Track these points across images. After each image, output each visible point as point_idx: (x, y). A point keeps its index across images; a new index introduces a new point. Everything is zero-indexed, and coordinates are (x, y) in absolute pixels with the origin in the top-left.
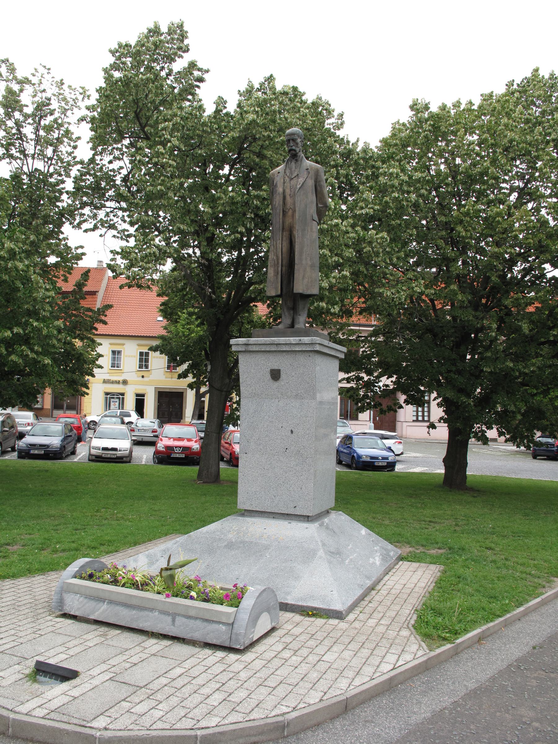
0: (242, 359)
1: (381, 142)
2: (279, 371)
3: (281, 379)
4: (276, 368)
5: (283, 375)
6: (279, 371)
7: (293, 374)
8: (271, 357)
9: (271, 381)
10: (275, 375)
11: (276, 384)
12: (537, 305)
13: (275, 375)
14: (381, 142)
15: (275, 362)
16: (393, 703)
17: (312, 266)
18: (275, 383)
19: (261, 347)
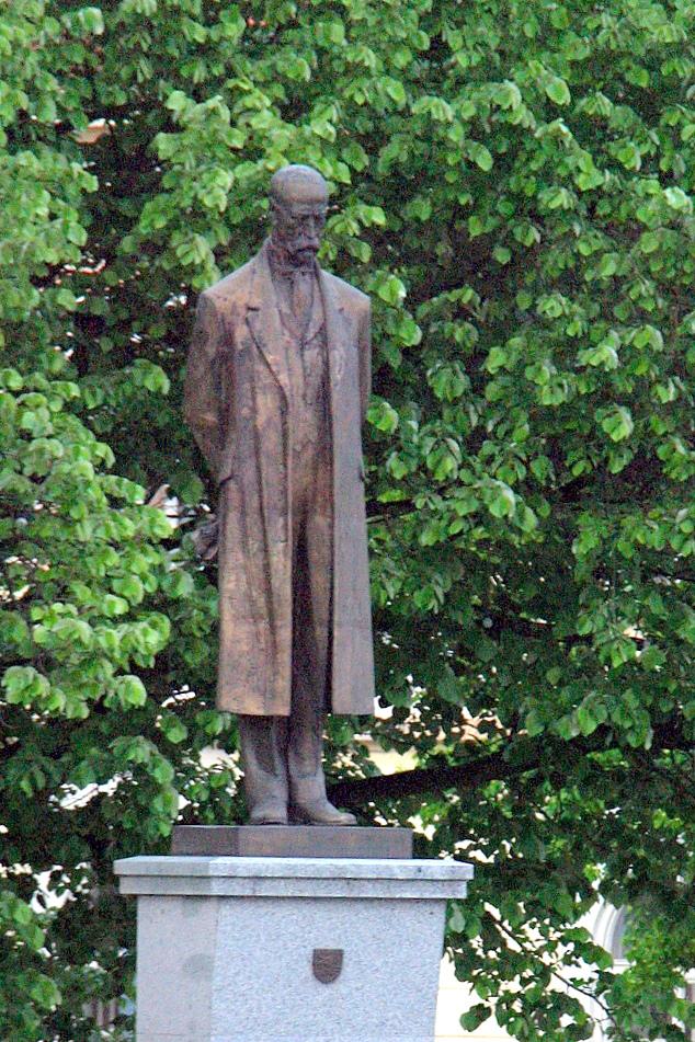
0: (144, 910)
1: (501, 1026)
2: (338, 955)
3: (341, 977)
4: (332, 946)
5: (348, 969)
6: (338, 955)
7: (378, 963)
8: (319, 913)
9: (312, 982)
10: (327, 966)
11: (326, 991)
12: (562, 927)
13: (327, 966)
14: (501, 1026)
15: (327, 928)
16: (509, 868)
17: (283, 127)
18: (322, 988)
19: (302, 884)
